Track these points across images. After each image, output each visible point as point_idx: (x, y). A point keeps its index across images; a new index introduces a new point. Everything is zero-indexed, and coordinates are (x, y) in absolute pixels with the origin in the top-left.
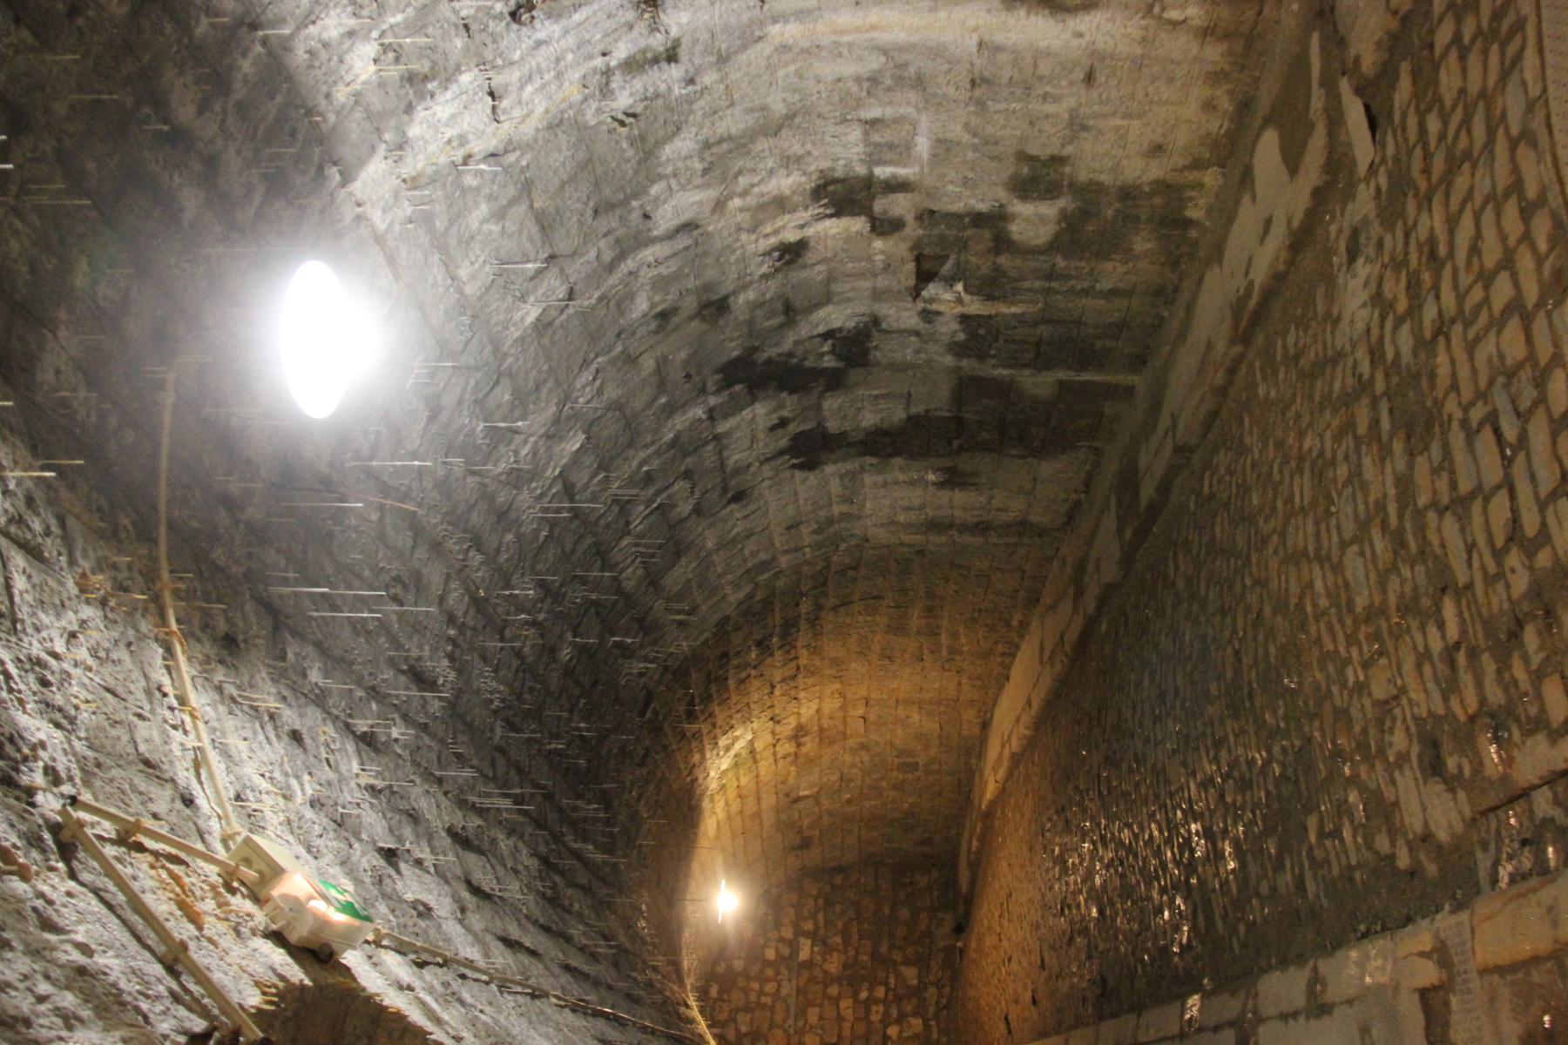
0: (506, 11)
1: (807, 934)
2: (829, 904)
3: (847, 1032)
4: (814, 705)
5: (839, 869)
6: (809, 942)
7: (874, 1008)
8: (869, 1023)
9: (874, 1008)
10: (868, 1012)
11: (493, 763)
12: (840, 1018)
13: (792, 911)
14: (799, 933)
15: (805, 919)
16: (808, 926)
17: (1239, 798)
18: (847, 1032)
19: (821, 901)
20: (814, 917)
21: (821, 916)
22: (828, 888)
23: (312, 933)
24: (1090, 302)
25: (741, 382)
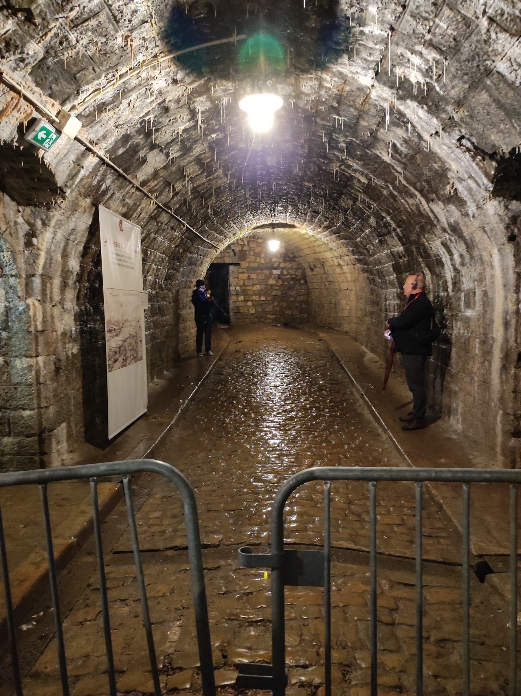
0: (463, 134)
1: (282, 272)
2: (293, 279)
3: (249, 288)
4: (347, 271)
5: (306, 282)
6: (279, 273)
7: (257, 297)
8: (252, 295)
9: (257, 297)
10: (256, 295)
11: (109, 110)
12: (253, 285)
13: (290, 266)
14: (283, 269)
15: (287, 271)
16: (285, 272)
17: (511, 25)
18: (249, 288)
19: (294, 276)
20: (288, 274)
21: (289, 276)
22: (299, 278)
23: (243, 112)
24: (432, 393)
25: (25, 631)
